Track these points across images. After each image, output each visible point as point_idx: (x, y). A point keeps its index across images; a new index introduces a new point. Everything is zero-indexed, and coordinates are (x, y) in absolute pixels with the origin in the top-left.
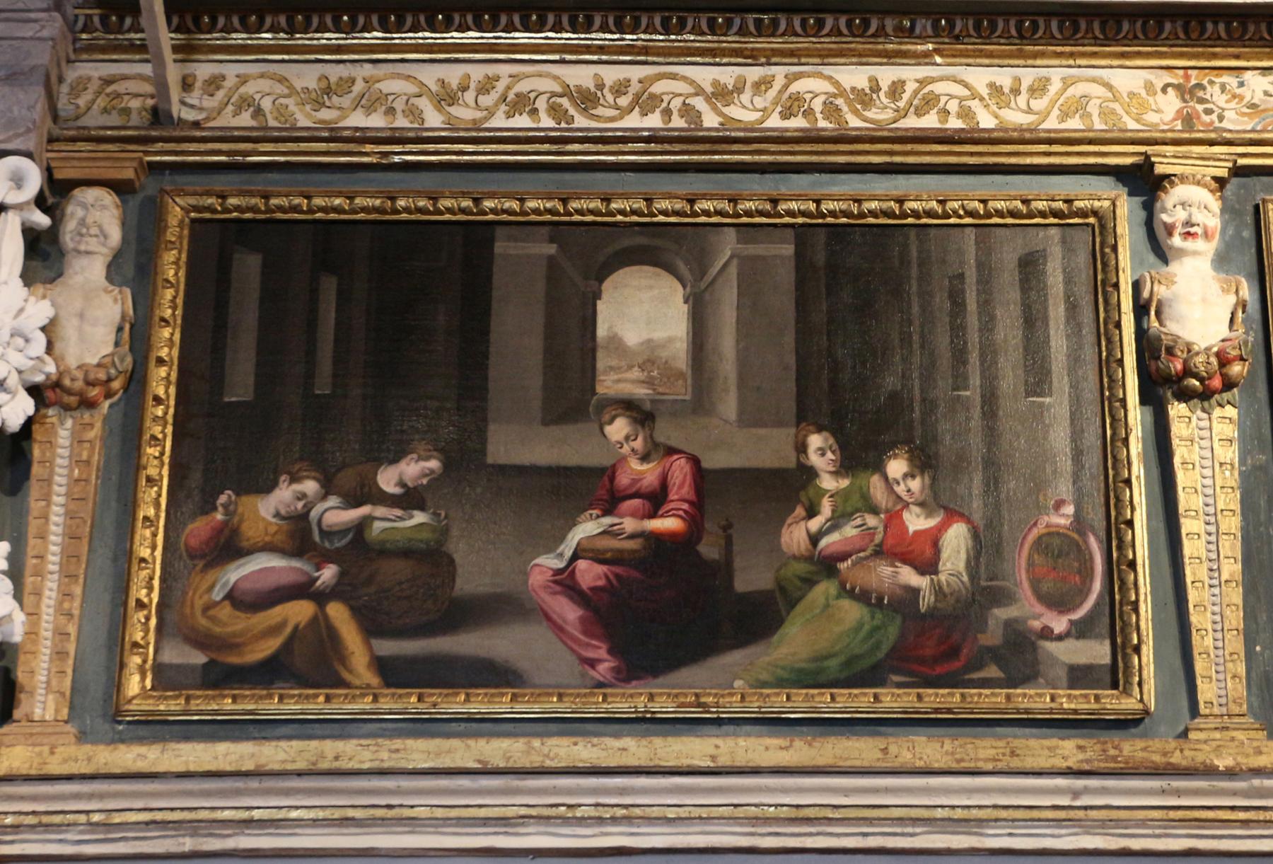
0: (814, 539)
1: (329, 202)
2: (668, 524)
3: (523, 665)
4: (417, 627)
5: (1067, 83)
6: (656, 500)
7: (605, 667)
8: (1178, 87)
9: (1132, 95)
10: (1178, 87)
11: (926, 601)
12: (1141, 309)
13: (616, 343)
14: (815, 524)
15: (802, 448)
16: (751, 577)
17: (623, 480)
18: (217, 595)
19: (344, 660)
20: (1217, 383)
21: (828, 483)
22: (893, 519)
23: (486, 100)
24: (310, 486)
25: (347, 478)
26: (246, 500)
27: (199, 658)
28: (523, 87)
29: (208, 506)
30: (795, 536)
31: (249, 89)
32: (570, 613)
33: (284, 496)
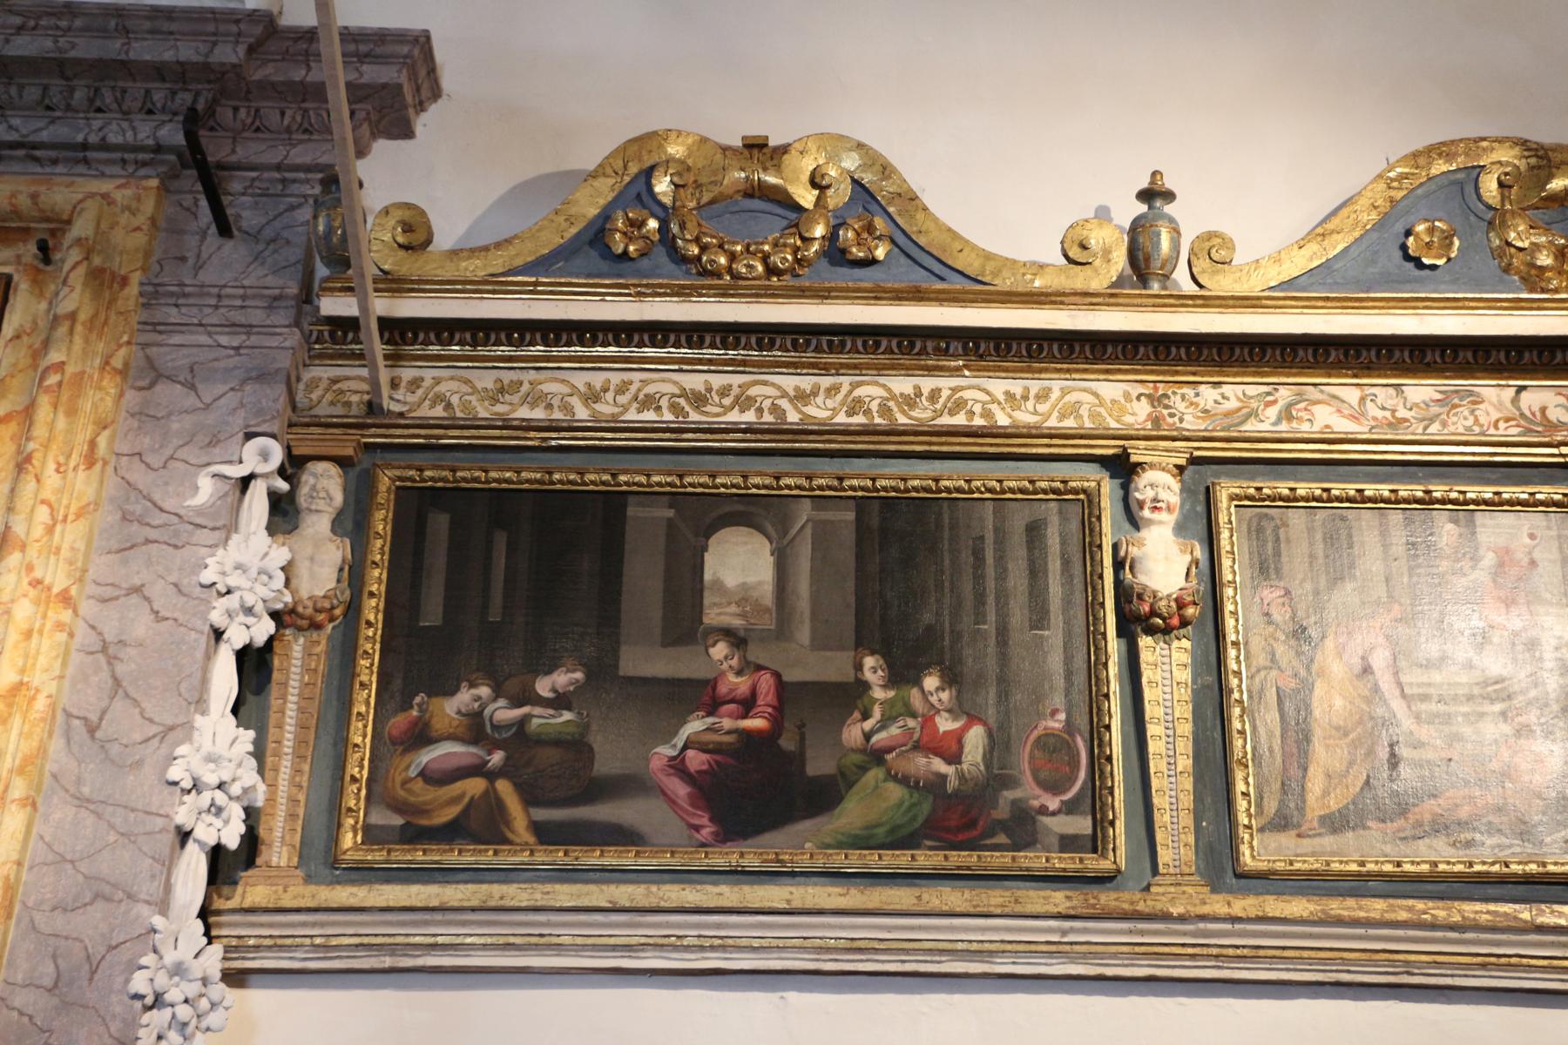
0: (867, 736)
1: (501, 475)
2: (756, 723)
3: (644, 829)
4: (564, 801)
5: (854, 386)
6: (747, 705)
7: (707, 831)
8: (1149, 396)
9: (1114, 401)
10: (1149, 396)
11: (952, 784)
12: (1118, 565)
13: (718, 585)
14: (868, 725)
15: (859, 667)
16: (819, 765)
17: (723, 689)
18: (413, 773)
19: (508, 824)
20: (1175, 621)
21: (878, 693)
22: (928, 721)
23: (622, 399)
24: (484, 691)
25: (512, 685)
26: (436, 701)
27: (398, 821)
28: (650, 389)
29: (406, 705)
30: (853, 733)
31: (442, 388)
32: (681, 790)
33: (464, 698)
